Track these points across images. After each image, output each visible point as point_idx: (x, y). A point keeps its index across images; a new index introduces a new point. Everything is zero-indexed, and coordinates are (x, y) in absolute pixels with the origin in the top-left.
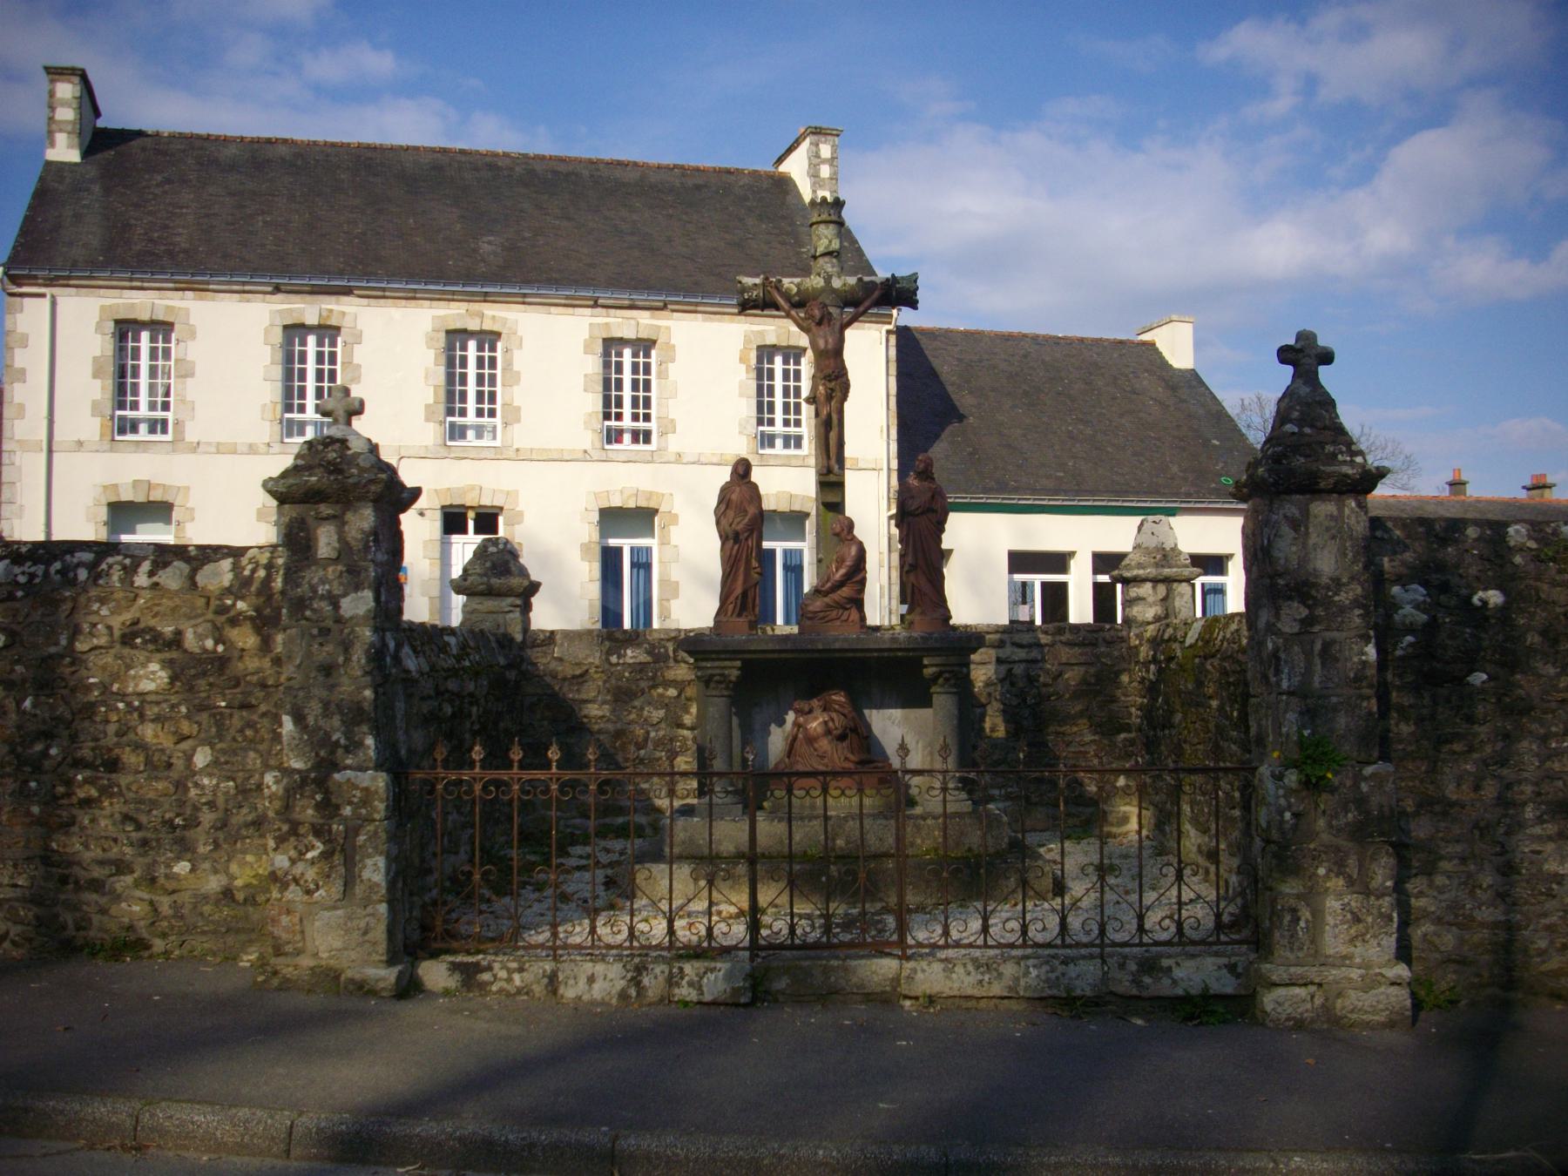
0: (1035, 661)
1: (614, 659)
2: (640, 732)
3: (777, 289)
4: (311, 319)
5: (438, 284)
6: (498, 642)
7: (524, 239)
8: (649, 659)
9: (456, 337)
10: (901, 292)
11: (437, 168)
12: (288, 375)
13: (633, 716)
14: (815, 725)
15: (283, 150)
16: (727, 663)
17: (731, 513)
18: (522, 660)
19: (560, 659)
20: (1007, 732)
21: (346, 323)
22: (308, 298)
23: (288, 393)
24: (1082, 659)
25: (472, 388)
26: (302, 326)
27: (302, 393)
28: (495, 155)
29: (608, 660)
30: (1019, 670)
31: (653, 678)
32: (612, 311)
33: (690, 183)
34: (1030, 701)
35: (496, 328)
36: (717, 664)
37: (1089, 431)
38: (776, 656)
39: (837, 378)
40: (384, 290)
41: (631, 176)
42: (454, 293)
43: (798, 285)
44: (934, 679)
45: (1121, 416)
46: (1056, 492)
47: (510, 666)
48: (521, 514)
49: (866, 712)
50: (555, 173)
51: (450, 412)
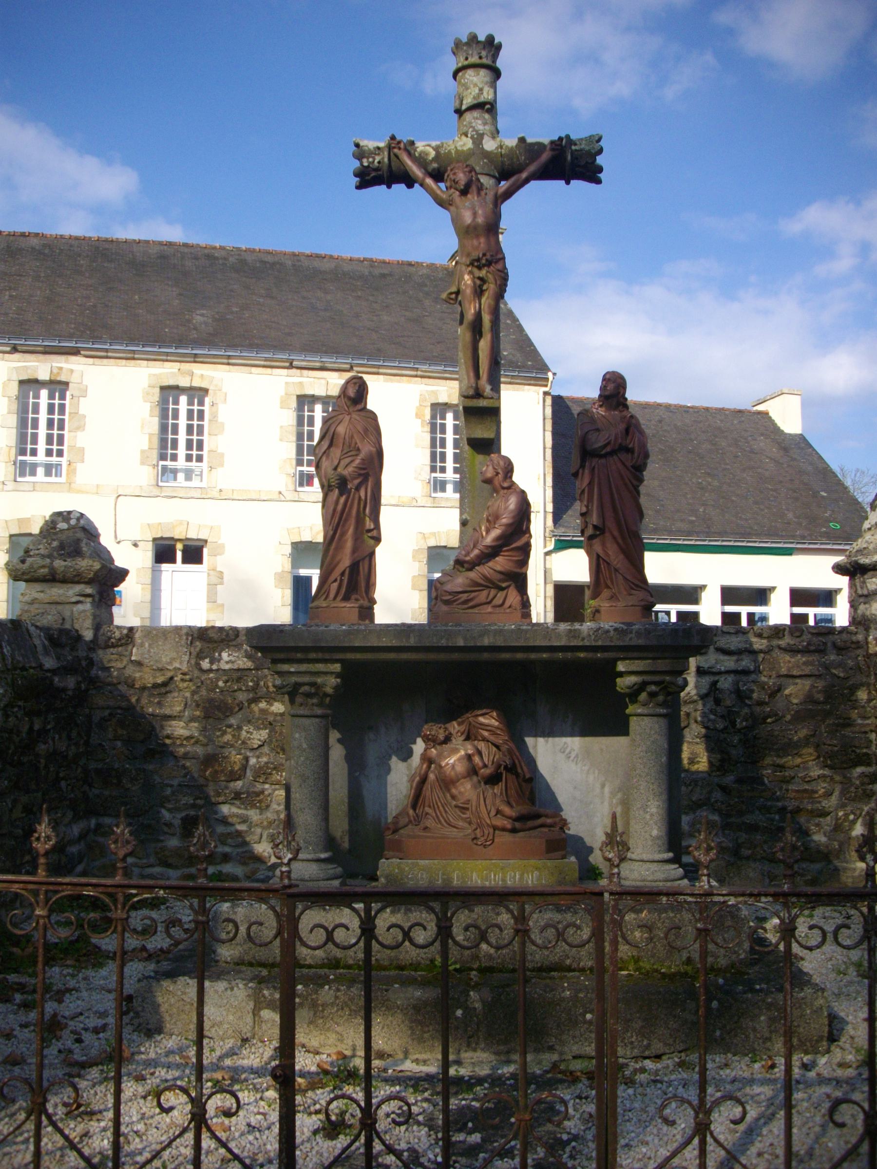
0: (745, 672)
1: (205, 664)
2: (236, 758)
3: (410, 154)
4: (43, 374)
5: (154, 346)
6: (50, 638)
7: (232, 313)
8: (249, 664)
9: (169, 392)
10: (578, 156)
11: (163, 257)
12: (23, 423)
13: (228, 737)
14: (453, 760)
15: (34, 242)
16: (320, 667)
17: (336, 453)
18: (91, 663)
19: (139, 664)
20: (710, 763)
21: (73, 379)
22: (41, 357)
23: (22, 438)
24: (807, 670)
25: (182, 437)
26: (36, 381)
27: (35, 439)
28: (215, 248)
29: (198, 665)
30: (726, 683)
31: (255, 689)
32: (305, 372)
33: (377, 272)
34: (740, 723)
35: (203, 385)
36: (304, 667)
37: (716, 483)
38: (392, 656)
39: (489, 264)
40: (107, 350)
41: (327, 266)
42: (167, 354)
43: (436, 149)
44: (634, 694)
45: (744, 470)
46: (689, 534)
47: (66, 670)
48: (222, 546)
49: (529, 741)
50: (262, 262)
51: (163, 457)
